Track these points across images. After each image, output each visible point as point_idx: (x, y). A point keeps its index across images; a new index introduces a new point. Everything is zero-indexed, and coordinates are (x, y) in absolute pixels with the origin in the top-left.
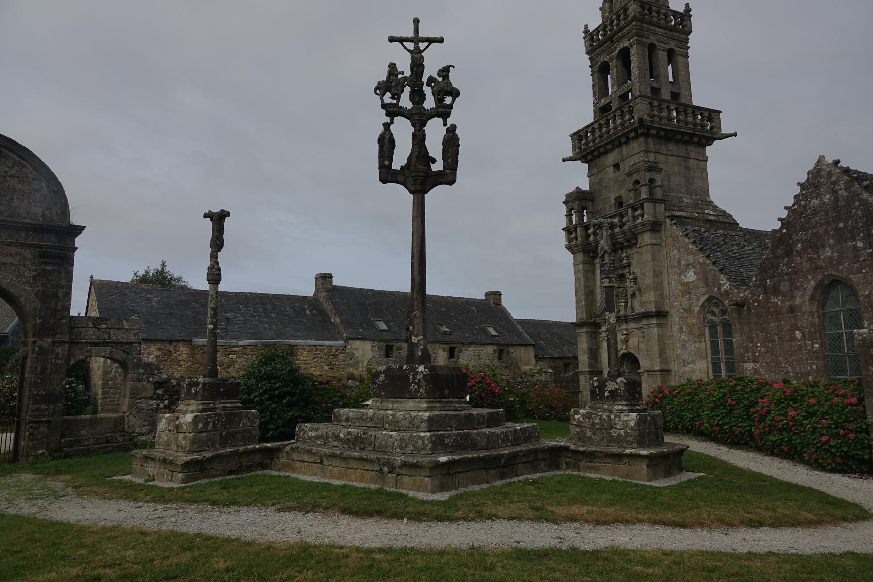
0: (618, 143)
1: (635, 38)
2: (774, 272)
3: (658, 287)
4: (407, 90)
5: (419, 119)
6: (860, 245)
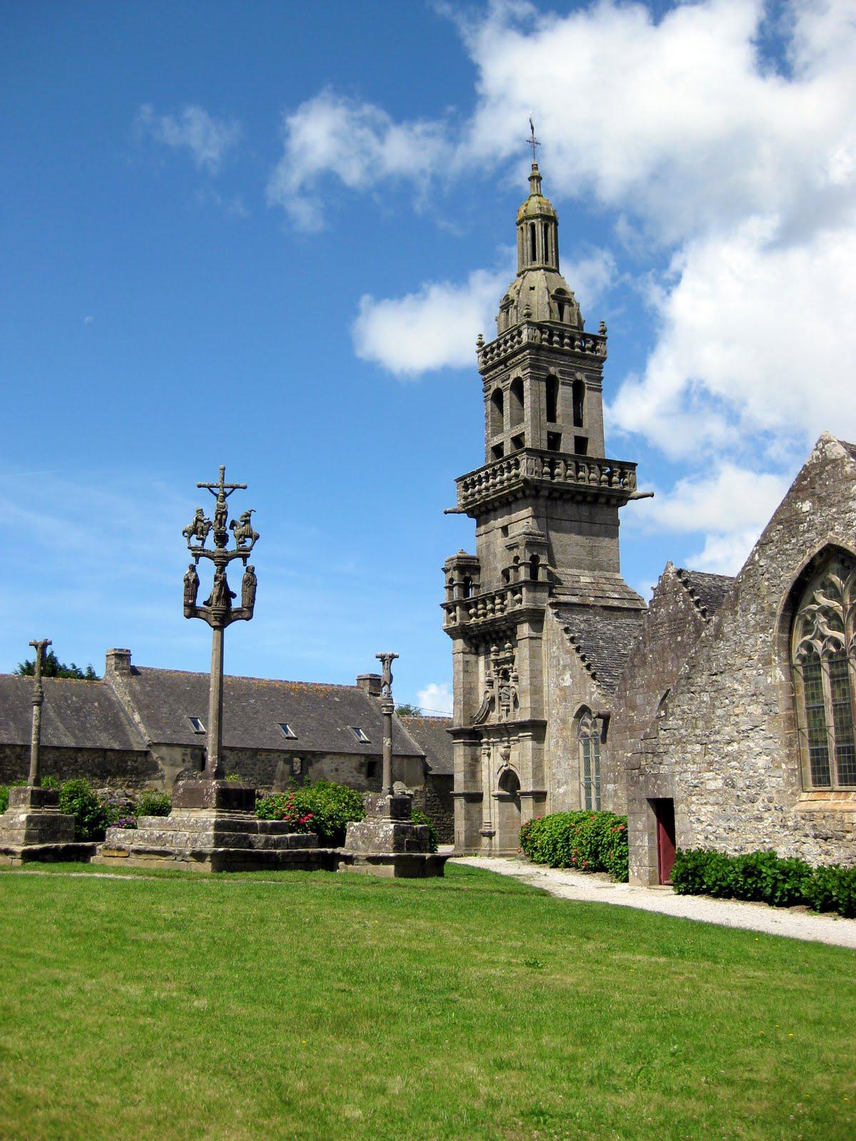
0: (506, 502)
1: (529, 370)
3: (536, 690)
4: (212, 534)
5: (223, 561)
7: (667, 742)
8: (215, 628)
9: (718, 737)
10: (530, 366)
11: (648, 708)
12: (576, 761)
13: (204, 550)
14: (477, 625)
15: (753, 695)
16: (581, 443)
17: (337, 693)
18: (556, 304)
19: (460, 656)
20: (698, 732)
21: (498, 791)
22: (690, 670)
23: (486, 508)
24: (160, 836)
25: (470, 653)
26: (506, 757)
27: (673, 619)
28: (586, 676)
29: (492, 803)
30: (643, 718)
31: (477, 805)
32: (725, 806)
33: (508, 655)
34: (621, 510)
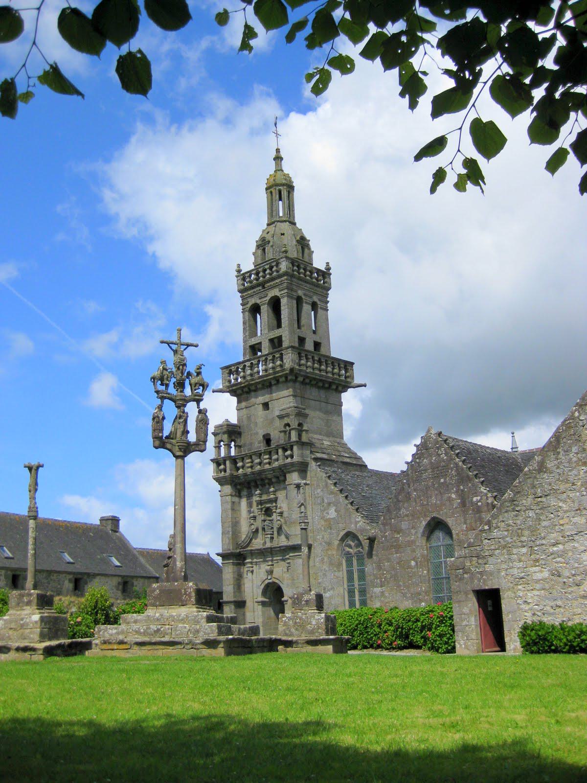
0: (268, 384)
2: (397, 513)
5: (181, 404)
6: (453, 496)
7: (493, 547)
8: (177, 457)
9: (544, 542)
10: (287, 288)
11: (413, 531)
12: (341, 573)
13: (169, 394)
14: (245, 475)
15: (577, 510)
16: (317, 345)
17: (90, 529)
18: (300, 247)
19: (229, 498)
20: (524, 539)
21: (261, 599)
22: (515, 495)
23: (249, 389)
24: (158, 630)
25: (235, 495)
26: (270, 572)
27: (434, 467)
28: (351, 510)
29: (255, 607)
30: (408, 538)
31: (242, 610)
32: (551, 591)
33: (272, 496)
34: (343, 394)
